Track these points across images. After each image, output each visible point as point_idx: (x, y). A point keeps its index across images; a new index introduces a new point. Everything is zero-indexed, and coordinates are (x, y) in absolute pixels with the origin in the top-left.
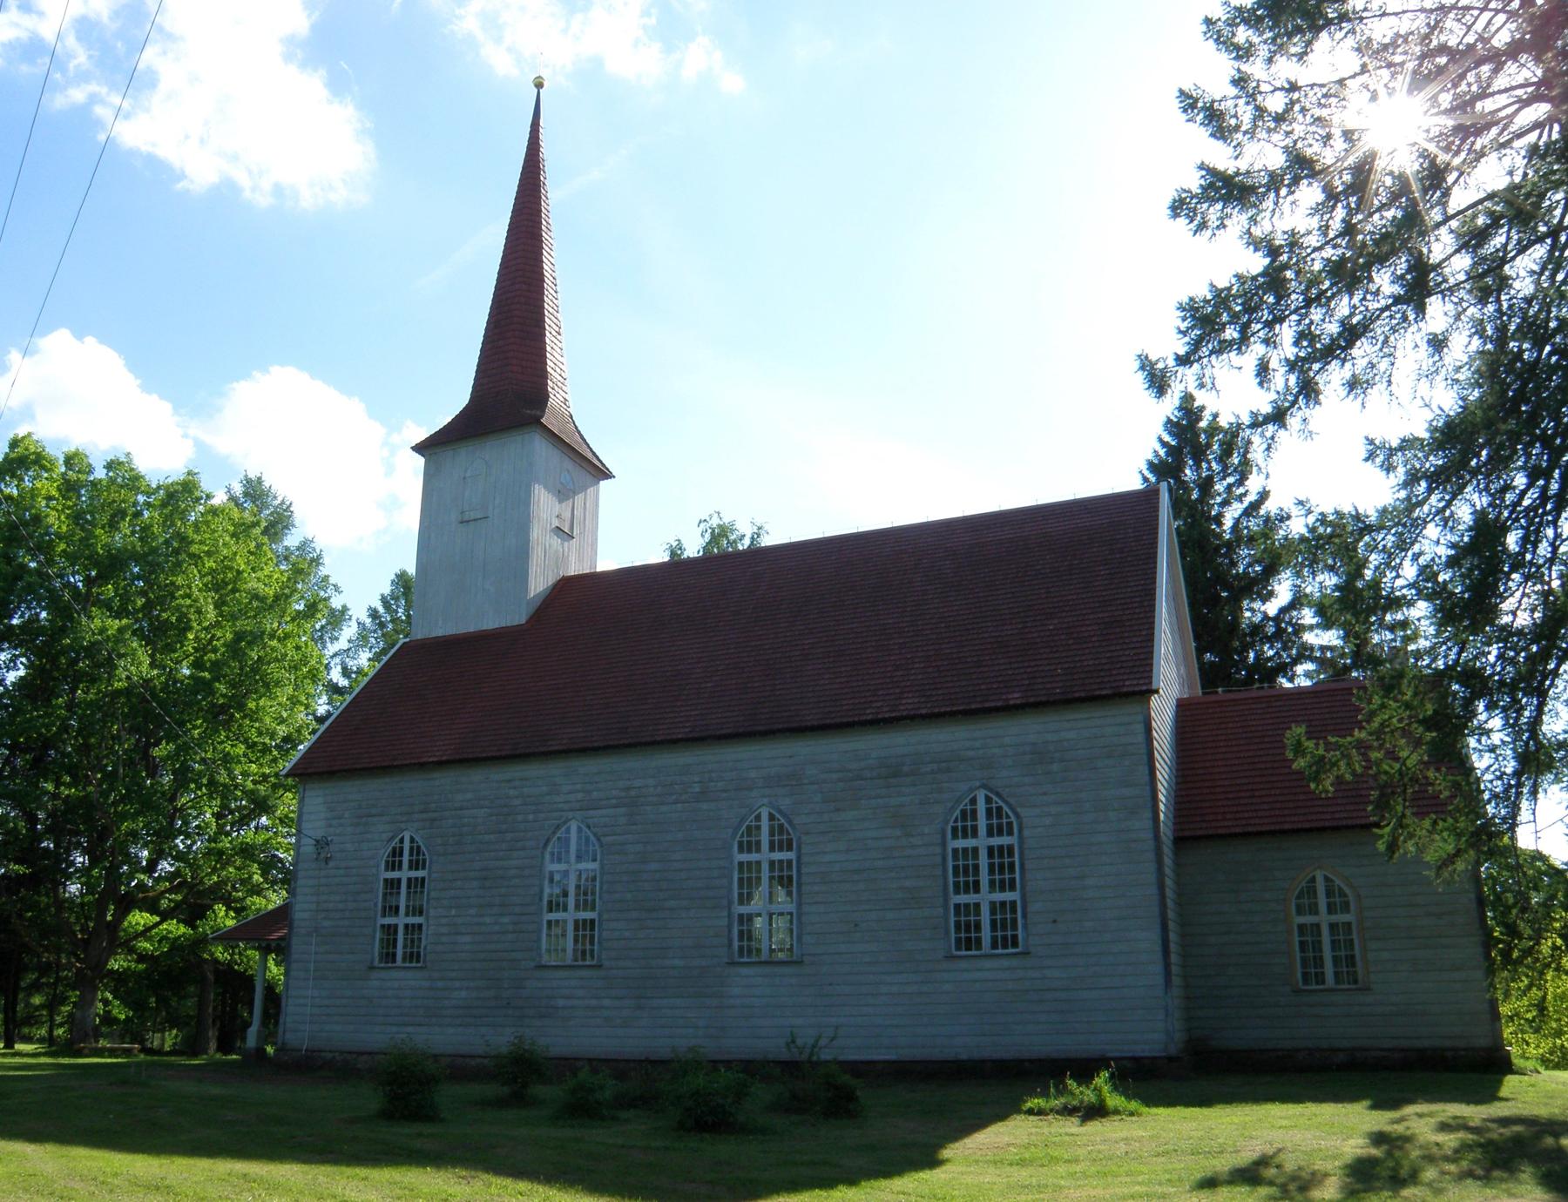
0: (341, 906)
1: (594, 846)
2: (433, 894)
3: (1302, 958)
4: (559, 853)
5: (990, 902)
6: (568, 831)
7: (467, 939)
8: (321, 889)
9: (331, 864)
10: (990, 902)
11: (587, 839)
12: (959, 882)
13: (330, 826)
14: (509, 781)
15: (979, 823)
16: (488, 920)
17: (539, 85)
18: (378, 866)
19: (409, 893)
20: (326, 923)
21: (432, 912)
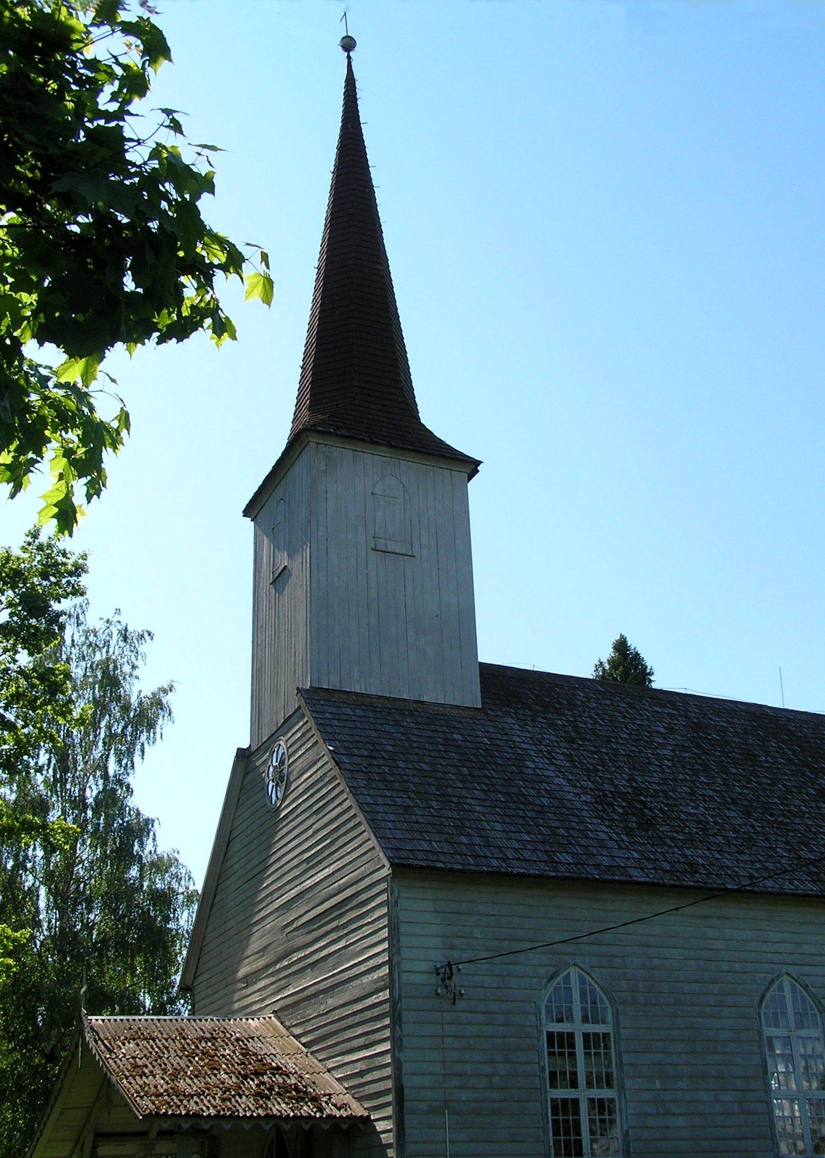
0: (486, 1069)
1: (812, 1009)
2: (626, 1059)
3: (553, 1120)
4: (775, 1014)
5: (577, 1087)
6: (781, 988)
7: (680, 1121)
8: (448, 1040)
9: (461, 1004)
10: (577, 1087)
11: (804, 1001)
12: (592, 1073)
13: (452, 947)
14: (705, 917)
15: (565, 1031)
16: (705, 1096)
17: (348, 44)
18: (538, 1014)
19: (588, 1054)
20: (464, 1095)
21: (628, 1083)
